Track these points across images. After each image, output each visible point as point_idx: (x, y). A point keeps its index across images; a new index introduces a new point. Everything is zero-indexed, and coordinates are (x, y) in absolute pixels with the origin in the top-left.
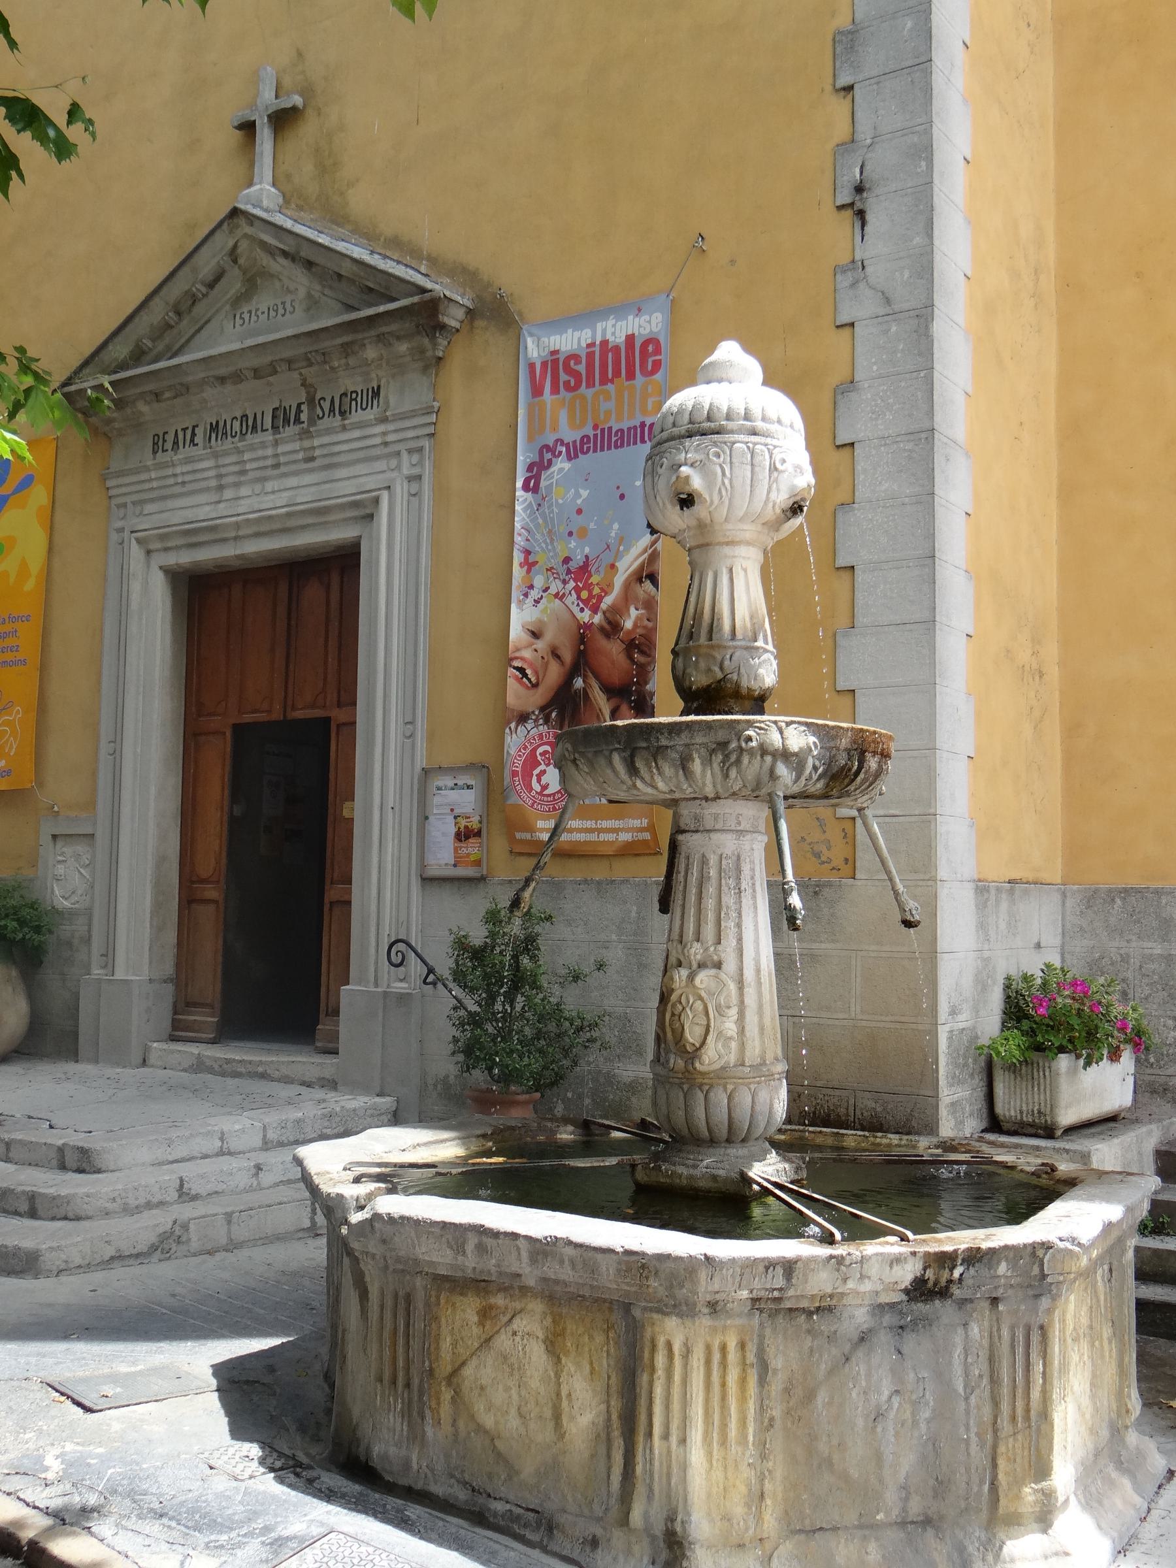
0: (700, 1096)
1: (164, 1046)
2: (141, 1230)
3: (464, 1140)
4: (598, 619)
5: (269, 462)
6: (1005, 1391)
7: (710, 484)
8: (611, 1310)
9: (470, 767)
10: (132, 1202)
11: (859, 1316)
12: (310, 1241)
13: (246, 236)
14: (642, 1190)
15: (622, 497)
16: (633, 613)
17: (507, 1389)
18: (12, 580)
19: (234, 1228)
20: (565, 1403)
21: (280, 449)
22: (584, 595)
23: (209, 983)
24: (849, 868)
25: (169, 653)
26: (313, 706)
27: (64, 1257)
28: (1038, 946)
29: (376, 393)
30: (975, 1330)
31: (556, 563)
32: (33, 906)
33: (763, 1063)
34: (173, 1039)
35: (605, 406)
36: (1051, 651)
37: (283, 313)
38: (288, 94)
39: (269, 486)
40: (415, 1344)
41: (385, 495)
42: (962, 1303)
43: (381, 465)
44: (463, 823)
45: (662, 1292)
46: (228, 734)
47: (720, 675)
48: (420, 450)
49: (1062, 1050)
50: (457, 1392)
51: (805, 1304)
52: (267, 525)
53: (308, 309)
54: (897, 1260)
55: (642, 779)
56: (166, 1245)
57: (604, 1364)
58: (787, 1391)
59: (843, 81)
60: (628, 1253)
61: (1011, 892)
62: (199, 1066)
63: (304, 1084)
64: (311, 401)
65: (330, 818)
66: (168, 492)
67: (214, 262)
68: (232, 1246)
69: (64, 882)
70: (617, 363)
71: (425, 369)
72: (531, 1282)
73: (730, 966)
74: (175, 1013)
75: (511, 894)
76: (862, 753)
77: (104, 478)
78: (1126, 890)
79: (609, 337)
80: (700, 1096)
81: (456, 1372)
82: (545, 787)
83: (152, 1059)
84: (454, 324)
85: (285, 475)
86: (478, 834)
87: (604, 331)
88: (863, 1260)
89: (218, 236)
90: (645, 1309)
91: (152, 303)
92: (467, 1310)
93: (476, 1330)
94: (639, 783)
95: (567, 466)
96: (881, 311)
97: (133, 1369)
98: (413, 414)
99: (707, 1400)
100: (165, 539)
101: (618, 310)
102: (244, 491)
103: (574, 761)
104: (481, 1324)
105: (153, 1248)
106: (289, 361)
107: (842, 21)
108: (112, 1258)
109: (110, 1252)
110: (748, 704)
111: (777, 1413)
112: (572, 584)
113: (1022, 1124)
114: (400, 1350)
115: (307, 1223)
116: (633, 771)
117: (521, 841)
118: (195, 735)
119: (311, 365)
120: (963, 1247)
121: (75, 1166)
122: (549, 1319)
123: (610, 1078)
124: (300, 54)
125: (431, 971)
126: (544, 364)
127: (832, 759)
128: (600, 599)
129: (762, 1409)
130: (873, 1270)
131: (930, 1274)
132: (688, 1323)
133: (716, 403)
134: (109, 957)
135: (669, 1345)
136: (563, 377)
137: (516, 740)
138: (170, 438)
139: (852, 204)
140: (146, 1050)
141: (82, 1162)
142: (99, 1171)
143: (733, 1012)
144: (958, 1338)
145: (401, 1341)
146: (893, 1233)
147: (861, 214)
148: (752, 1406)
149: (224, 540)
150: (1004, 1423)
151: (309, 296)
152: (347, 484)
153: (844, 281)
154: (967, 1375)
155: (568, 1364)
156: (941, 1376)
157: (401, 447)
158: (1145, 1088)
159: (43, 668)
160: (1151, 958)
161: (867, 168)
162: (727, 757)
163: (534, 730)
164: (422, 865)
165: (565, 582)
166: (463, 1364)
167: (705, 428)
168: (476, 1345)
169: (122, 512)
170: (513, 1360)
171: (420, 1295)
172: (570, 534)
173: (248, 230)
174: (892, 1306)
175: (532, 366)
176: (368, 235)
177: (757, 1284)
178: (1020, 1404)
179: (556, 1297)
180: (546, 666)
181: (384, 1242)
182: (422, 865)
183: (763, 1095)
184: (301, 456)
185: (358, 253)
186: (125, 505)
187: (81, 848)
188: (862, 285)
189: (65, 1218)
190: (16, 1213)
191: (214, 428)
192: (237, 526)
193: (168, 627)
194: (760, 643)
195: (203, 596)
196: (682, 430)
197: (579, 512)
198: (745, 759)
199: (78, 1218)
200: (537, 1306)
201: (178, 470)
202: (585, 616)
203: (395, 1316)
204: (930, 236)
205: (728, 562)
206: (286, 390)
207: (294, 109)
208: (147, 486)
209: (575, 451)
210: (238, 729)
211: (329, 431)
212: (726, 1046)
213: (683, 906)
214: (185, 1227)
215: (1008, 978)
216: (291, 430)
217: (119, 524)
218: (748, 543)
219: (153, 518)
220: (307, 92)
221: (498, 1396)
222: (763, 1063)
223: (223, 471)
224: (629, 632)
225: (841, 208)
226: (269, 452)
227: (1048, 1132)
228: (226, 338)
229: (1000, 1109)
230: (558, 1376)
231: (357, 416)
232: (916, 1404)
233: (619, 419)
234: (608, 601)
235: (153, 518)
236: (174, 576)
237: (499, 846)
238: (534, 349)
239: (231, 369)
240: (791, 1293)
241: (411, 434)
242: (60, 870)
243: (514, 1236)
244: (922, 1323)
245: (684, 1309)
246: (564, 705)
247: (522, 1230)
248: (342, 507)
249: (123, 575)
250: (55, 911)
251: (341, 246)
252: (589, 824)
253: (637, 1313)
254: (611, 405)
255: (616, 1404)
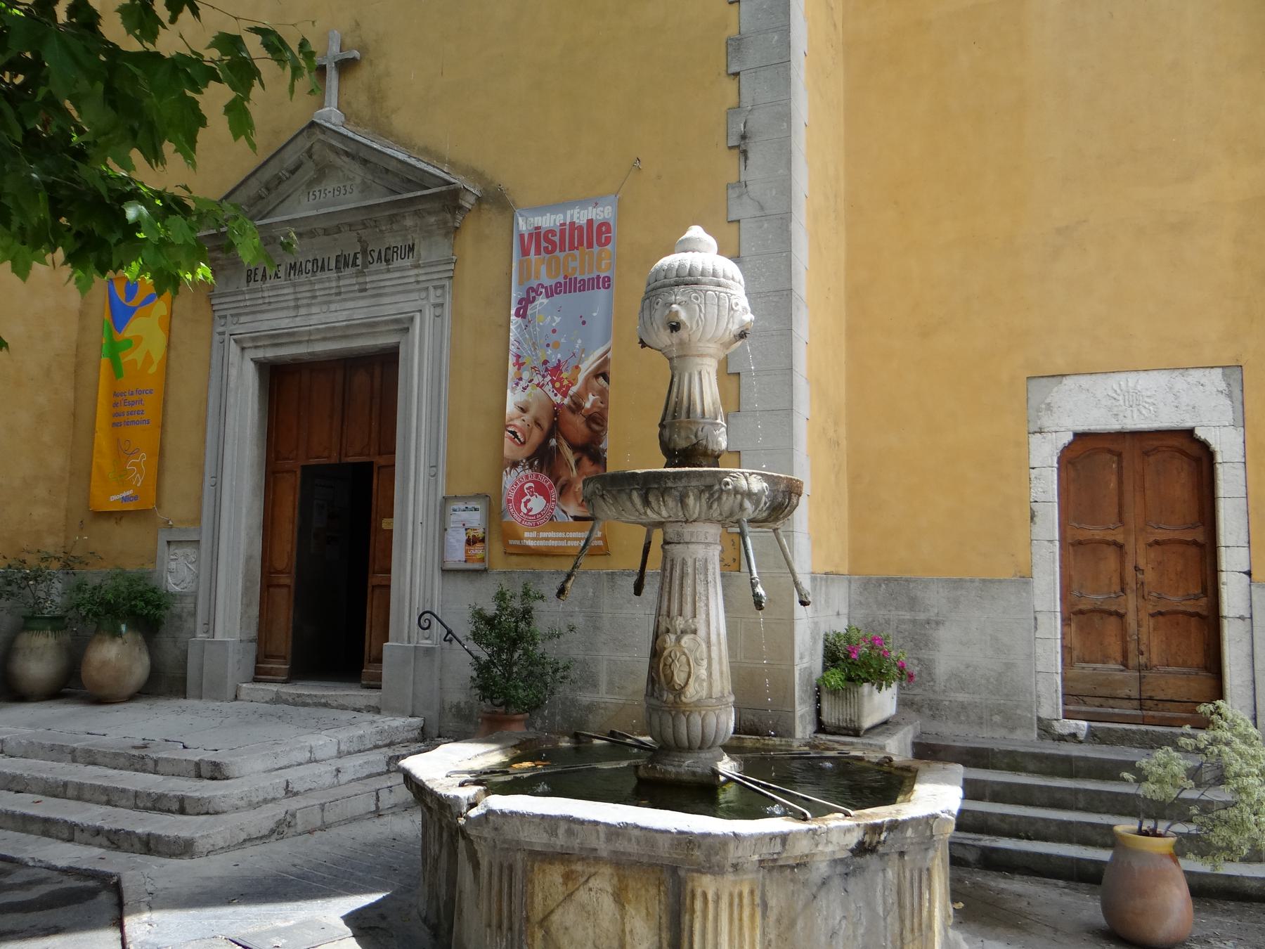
0: (684, 719)
1: (251, 686)
2: (264, 819)
3: (504, 750)
4: (566, 401)
5: (333, 291)
6: (908, 912)
7: (691, 318)
8: (662, 871)
9: (477, 497)
10: (255, 800)
11: (822, 868)
12: (376, 820)
13: (319, 140)
14: (641, 782)
15: (584, 323)
16: (591, 398)
17: (585, 929)
18: (139, 365)
19: (326, 814)
20: (628, 937)
21: (341, 283)
22: (557, 385)
23: (283, 641)
24: (736, 564)
25: (256, 417)
26: (361, 454)
27: (211, 842)
28: (838, 614)
29: (411, 249)
30: (890, 874)
31: (538, 363)
32: (154, 590)
33: (723, 696)
34: (255, 680)
35: (572, 264)
36: (843, 430)
37: (344, 194)
38: (350, 49)
39: (333, 307)
40: (516, 901)
41: (418, 316)
42: (883, 856)
43: (414, 296)
44: (472, 533)
45: (702, 858)
46: (299, 473)
47: (695, 441)
48: (443, 287)
49: (868, 681)
50: (547, 932)
51: (791, 862)
52: (330, 333)
53: (362, 191)
54: (848, 830)
55: (652, 509)
56: (280, 830)
57: (656, 908)
58: (779, 921)
59: (733, 69)
60: (680, 833)
61: (826, 580)
62: (277, 700)
63: (355, 710)
64: (364, 252)
65: (373, 529)
66: (258, 308)
67: (295, 157)
68: (324, 827)
69: (177, 573)
70: (581, 237)
71: (446, 235)
72: (605, 854)
73: (702, 632)
74: (257, 662)
75: (558, 583)
76: (790, 493)
77: (210, 298)
78: (888, 580)
79: (575, 220)
80: (684, 719)
81: (546, 918)
82: (530, 510)
83: (242, 695)
84: (468, 206)
85: (345, 300)
86: (483, 540)
87: (572, 216)
88: (829, 831)
89: (300, 140)
90: (688, 870)
91: (249, 182)
92: (554, 874)
93: (561, 889)
94: (649, 512)
95: (545, 301)
96: (758, 213)
97: (287, 924)
98: (438, 263)
99: (730, 931)
100: (256, 340)
101: (583, 203)
102: (314, 310)
103: (602, 496)
104: (565, 883)
105: (272, 831)
106: (350, 225)
107: (732, 31)
108: (245, 841)
109: (243, 836)
110: (711, 460)
111: (772, 936)
112: (549, 378)
113: (839, 728)
114: (505, 905)
115: (373, 808)
116: (646, 503)
117: (513, 546)
118: (274, 473)
119: (366, 227)
120: (887, 819)
121: (209, 775)
122: (616, 879)
123: (574, 702)
124: (358, 24)
125: (449, 632)
126: (531, 235)
127: (775, 497)
128: (568, 388)
129: (764, 934)
130: (834, 837)
131: (867, 839)
132: (719, 878)
133: (695, 264)
134: (210, 626)
135: (705, 895)
136: (544, 244)
137: (510, 479)
138: (260, 273)
139: (738, 147)
140: (238, 688)
141: (216, 772)
142: (227, 778)
143: (705, 663)
144: (879, 879)
145: (505, 897)
146: (839, 811)
147: (745, 153)
148: (758, 932)
149: (300, 342)
150: (907, 934)
151: (364, 182)
152: (390, 307)
153: (733, 194)
154: (885, 903)
155: (630, 909)
156: (870, 905)
157: (430, 285)
158: (903, 703)
159: (163, 426)
160: (903, 621)
161: (749, 124)
162: (712, 495)
163: (522, 473)
164: (443, 561)
165: (544, 376)
166: (552, 912)
167: (687, 280)
168: (561, 898)
169: (223, 322)
170: (589, 908)
171: (519, 866)
172: (548, 345)
173: (322, 137)
174: (842, 860)
175: (522, 236)
176: (407, 146)
177: (764, 851)
178: (916, 920)
179: (620, 863)
180: (531, 431)
181: (496, 829)
182: (443, 561)
183: (723, 718)
184: (357, 287)
185: (401, 156)
186: (225, 317)
187: (189, 550)
188: (745, 197)
189: (207, 813)
190: (169, 811)
191: (293, 267)
192: (310, 333)
193: (256, 399)
194: (719, 421)
195: (278, 378)
196: (672, 281)
197: (554, 331)
198: (724, 497)
199: (217, 813)
200: (607, 870)
201: (266, 294)
202: (558, 399)
203: (501, 881)
204: (789, 169)
205: (699, 368)
206: (348, 243)
207: (354, 59)
208: (242, 304)
209: (551, 292)
210: (305, 469)
211: (377, 272)
212: (701, 685)
213: (670, 593)
214: (294, 816)
215: (826, 635)
216: (350, 270)
217: (221, 329)
218: (711, 356)
219: (246, 326)
220: (363, 49)
221: (578, 934)
222: (723, 696)
223: (299, 296)
224: (588, 410)
225: (730, 148)
226: (334, 284)
227: (856, 732)
228: (303, 207)
229: (824, 718)
230: (623, 918)
231: (397, 263)
232: (855, 925)
233: (582, 273)
234: (573, 390)
235: (246, 326)
236: (261, 365)
237: (497, 548)
238: (524, 225)
239: (309, 228)
240: (784, 855)
241: (435, 276)
242: (173, 565)
243: (596, 823)
244: (861, 869)
245: (716, 870)
246: (544, 458)
247: (601, 819)
248: (386, 323)
249: (224, 364)
250: (173, 595)
251: (389, 151)
252: (560, 535)
253: (682, 873)
254: (576, 264)
255: (665, 936)
